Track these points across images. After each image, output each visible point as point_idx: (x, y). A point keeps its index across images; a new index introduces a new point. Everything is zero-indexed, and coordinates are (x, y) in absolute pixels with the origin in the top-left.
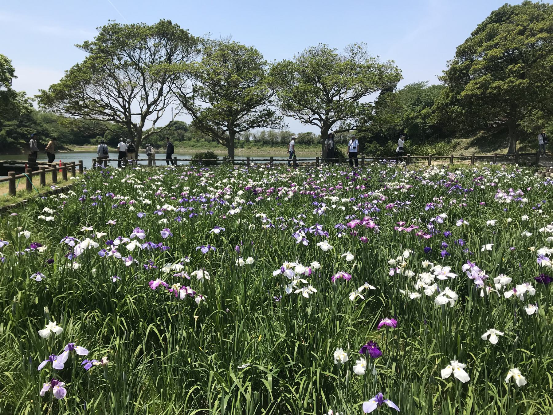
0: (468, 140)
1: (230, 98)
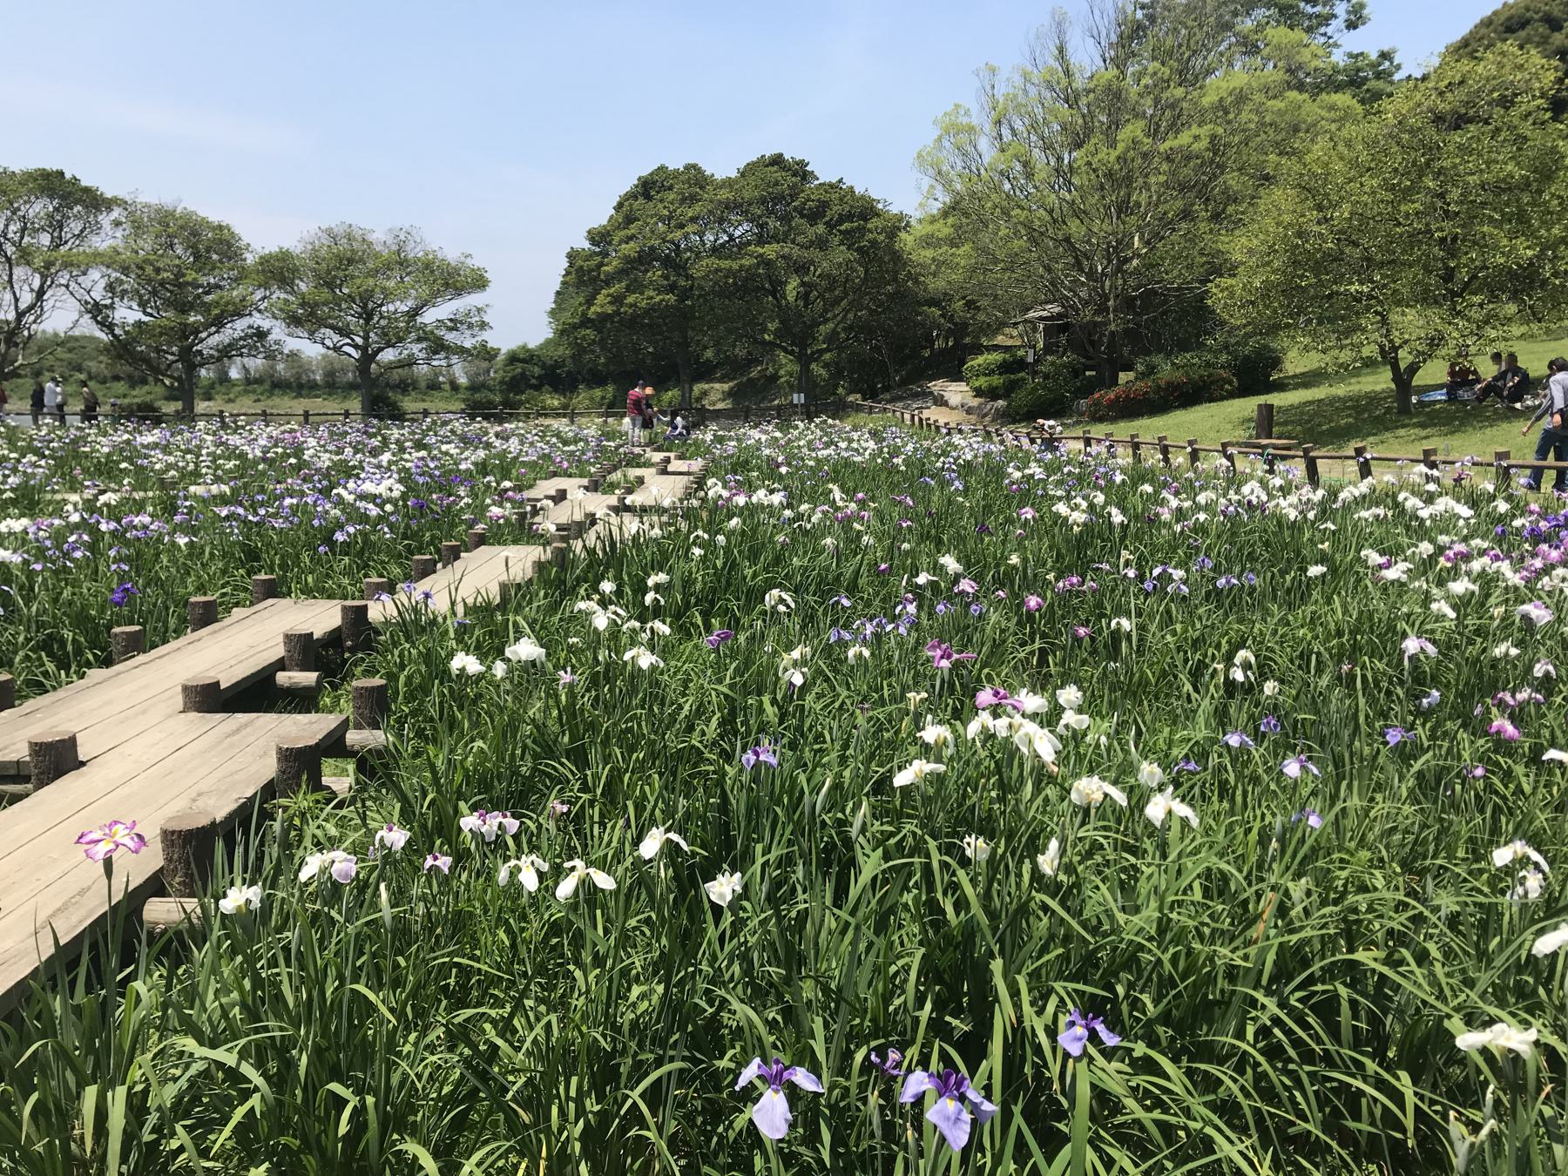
0: (726, 387)
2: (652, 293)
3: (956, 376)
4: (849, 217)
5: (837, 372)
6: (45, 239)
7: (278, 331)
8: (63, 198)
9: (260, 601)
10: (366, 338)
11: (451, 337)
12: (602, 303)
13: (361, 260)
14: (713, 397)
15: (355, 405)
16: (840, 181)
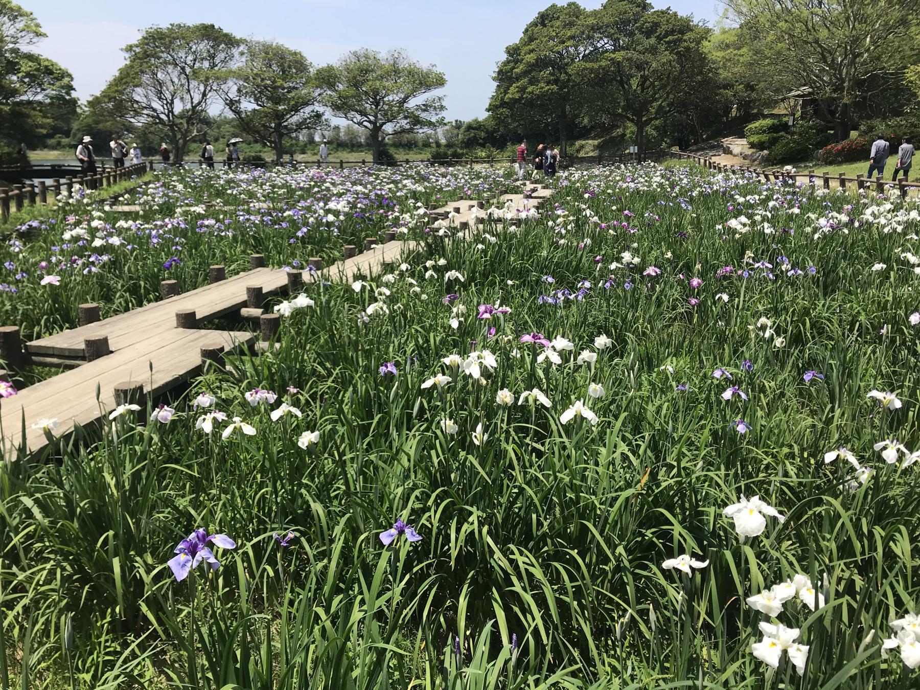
0: (596, 142)
1: (277, 101)
2: (543, 85)
3: (742, 136)
4: (672, 32)
5: (662, 131)
6: (206, 64)
7: (328, 114)
8: (215, 40)
9: (254, 268)
10: (376, 116)
11: (424, 116)
12: (513, 92)
13: (372, 71)
14: (588, 149)
15: (369, 157)
16: (669, 9)
